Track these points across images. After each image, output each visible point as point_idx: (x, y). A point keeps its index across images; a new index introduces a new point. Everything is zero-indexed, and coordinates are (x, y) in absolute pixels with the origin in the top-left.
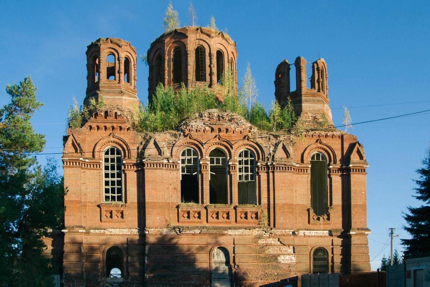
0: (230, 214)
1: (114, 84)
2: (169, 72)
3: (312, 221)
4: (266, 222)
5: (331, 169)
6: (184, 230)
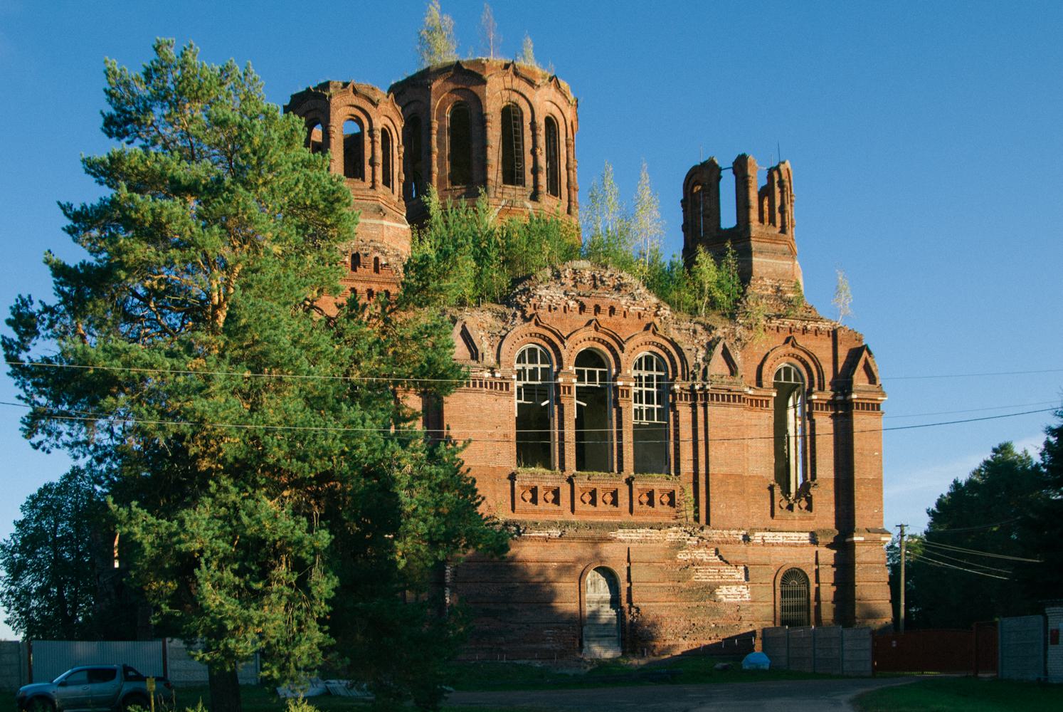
0: (619, 496)
1: (362, 190)
2: (440, 157)
3: (777, 511)
4: (690, 513)
5: (854, 401)
6: (528, 530)
